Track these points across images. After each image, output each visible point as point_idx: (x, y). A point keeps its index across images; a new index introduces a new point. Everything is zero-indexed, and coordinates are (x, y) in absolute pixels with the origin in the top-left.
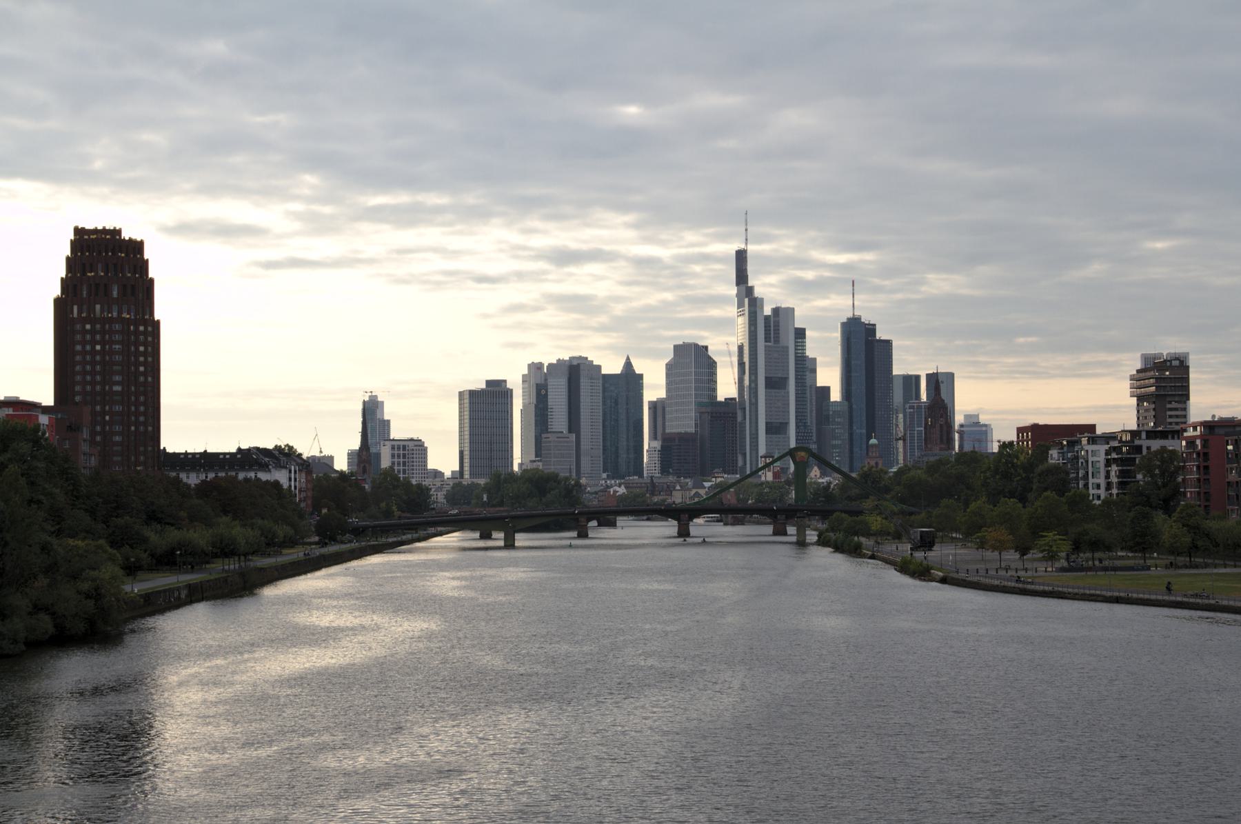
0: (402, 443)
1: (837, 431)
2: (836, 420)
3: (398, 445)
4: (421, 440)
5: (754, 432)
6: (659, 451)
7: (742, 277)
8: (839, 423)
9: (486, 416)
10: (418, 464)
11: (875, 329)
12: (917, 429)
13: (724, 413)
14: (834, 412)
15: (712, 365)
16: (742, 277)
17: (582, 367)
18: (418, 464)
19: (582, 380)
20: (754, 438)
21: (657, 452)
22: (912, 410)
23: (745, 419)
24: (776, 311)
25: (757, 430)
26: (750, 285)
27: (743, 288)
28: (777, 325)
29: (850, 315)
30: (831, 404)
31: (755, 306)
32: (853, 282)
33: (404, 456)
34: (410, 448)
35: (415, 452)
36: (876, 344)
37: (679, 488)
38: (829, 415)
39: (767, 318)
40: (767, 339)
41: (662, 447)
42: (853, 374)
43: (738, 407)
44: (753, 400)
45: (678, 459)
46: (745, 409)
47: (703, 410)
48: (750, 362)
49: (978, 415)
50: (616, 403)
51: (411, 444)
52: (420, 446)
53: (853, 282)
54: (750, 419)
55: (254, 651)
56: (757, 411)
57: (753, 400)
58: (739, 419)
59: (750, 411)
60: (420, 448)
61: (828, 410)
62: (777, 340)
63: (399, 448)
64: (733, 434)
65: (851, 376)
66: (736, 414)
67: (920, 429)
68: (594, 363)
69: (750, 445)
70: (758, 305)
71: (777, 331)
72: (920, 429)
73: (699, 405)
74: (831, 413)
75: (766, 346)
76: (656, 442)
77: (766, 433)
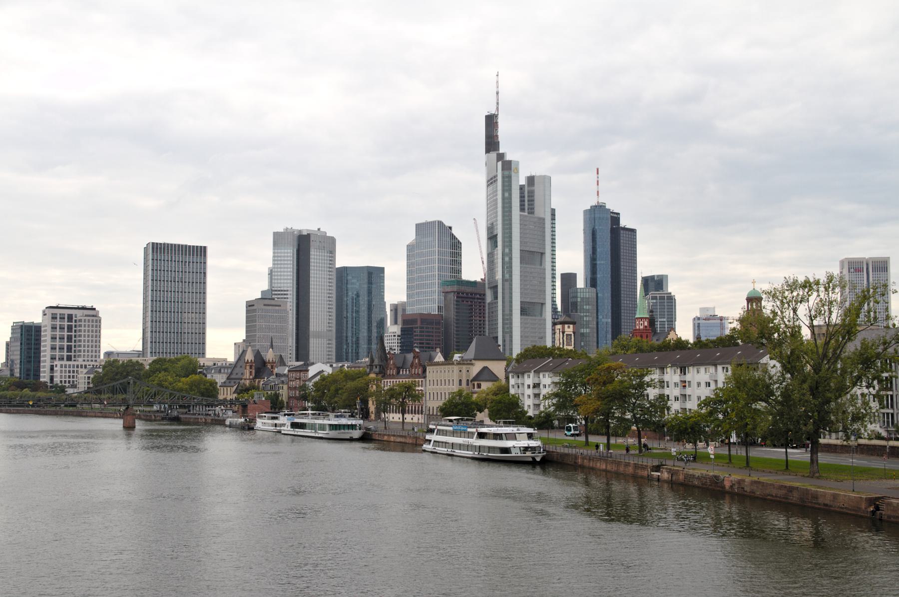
0: (67, 312)
1: (585, 319)
2: (585, 307)
3: (68, 315)
4: (95, 309)
5: (507, 312)
6: (398, 336)
7: (492, 143)
8: (588, 311)
9: (175, 277)
10: (87, 333)
11: (619, 218)
12: (665, 320)
13: (471, 294)
14: (582, 299)
15: (456, 245)
16: (492, 143)
17: (312, 238)
18: (87, 333)
19: (312, 252)
20: (507, 319)
21: (396, 337)
22: (655, 301)
23: (496, 298)
24: (531, 180)
25: (511, 311)
26: (501, 151)
27: (493, 155)
28: (531, 194)
29: (594, 203)
30: (579, 291)
31: (510, 169)
32: (598, 169)
33: (70, 328)
34: (78, 318)
35: (83, 323)
36: (622, 232)
37: (442, 359)
38: (577, 302)
39: (522, 188)
40: (522, 209)
41: (403, 330)
42: (598, 262)
43: (487, 286)
44: (507, 276)
45: (420, 343)
46: (496, 287)
47: (449, 289)
48: (504, 233)
49: (714, 308)
50: (358, 295)
51: (79, 313)
52: (93, 316)
53: (598, 169)
54: (503, 298)
55: (495, 394)
56: (511, 289)
57: (507, 276)
58: (489, 298)
59: (503, 289)
60: (94, 318)
61: (577, 297)
62: (531, 211)
63: (62, 318)
64: (480, 317)
65: (596, 264)
66: (484, 295)
67: (662, 320)
68: (328, 235)
69: (503, 328)
70: (513, 169)
71: (531, 201)
72: (662, 320)
73: (445, 284)
74: (579, 300)
75: (521, 215)
76: (396, 326)
77: (521, 314)
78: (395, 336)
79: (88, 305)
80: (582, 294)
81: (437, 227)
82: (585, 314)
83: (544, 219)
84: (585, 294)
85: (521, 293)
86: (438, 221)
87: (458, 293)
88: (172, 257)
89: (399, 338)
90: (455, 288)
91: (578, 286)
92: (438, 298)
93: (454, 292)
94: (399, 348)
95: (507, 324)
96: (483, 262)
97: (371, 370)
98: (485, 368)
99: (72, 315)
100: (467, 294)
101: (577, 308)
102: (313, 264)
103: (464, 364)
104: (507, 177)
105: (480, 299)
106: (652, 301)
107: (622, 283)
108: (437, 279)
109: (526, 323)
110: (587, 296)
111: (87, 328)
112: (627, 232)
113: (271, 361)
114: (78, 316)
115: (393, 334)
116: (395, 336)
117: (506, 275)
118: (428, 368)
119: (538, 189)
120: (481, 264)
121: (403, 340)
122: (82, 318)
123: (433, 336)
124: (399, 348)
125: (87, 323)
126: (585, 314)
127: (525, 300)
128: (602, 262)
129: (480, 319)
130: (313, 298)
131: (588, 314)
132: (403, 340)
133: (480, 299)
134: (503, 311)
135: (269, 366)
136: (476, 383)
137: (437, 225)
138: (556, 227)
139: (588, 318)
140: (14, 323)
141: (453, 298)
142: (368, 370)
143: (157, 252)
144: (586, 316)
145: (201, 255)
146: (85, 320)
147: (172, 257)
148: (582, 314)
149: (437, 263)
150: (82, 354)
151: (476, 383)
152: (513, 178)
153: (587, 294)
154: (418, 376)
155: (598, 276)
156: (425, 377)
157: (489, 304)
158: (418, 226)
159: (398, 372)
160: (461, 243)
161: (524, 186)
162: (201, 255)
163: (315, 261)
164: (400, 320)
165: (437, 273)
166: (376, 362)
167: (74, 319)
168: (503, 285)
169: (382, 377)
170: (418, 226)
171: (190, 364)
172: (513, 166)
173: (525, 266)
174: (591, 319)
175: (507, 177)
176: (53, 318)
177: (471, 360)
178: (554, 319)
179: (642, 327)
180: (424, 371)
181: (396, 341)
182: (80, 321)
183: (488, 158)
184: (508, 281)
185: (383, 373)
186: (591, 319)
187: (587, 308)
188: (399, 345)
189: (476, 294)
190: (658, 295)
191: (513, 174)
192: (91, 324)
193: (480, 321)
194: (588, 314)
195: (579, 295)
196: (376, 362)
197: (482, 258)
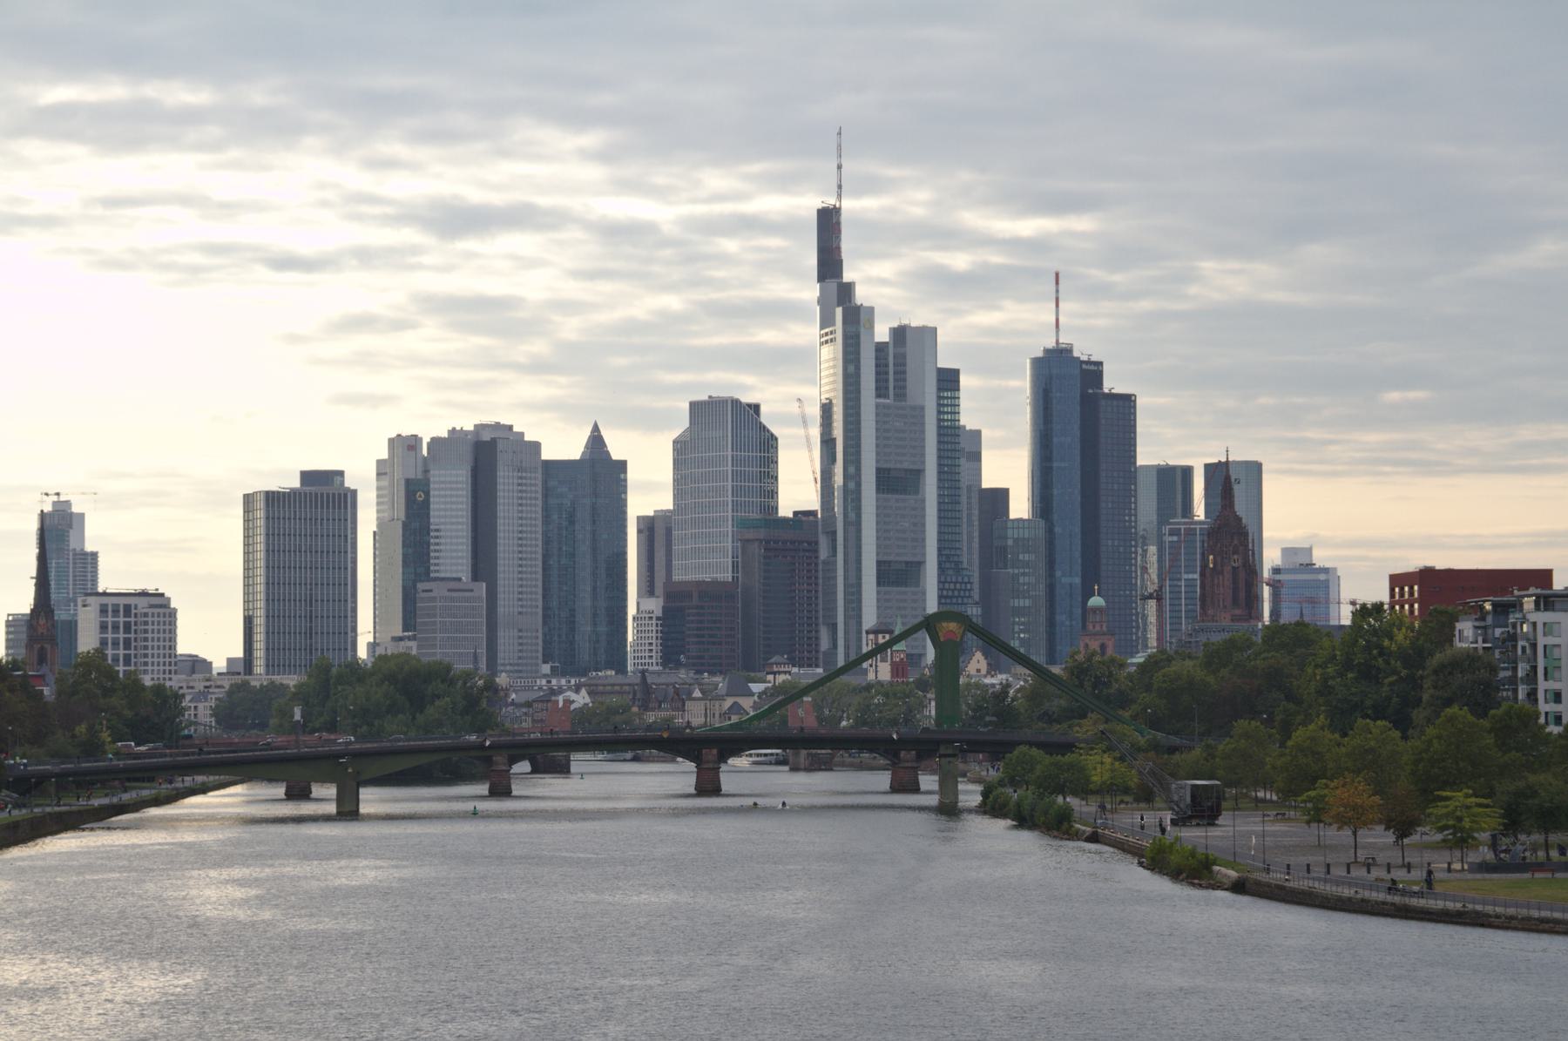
0: (122, 601)
1: (1021, 580)
2: (1021, 557)
4: (162, 595)
6: (658, 619)
7: (829, 264)
8: (1027, 564)
11: (1102, 371)
12: (1185, 576)
13: (793, 542)
14: (1016, 540)
15: (767, 444)
17: (500, 446)
19: (500, 473)
21: (654, 622)
22: (1175, 538)
24: (900, 333)
25: (859, 578)
27: (832, 285)
28: (901, 362)
29: (1051, 344)
30: (1010, 525)
31: (857, 322)
32: (1057, 275)
34: (141, 610)
36: (1103, 402)
37: (700, 695)
39: (881, 348)
40: (881, 391)
42: (1055, 465)
44: (852, 516)
46: (834, 533)
47: (750, 535)
53: (1057, 275)
54: (846, 554)
58: (823, 554)
59: (845, 539)
61: (1006, 538)
62: (901, 394)
63: (116, 612)
66: (817, 543)
67: (1191, 576)
71: (901, 374)
72: (1191, 576)
73: (742, 524)
74: (1010, 542)
77: (879, 584)
78: (651, 618)
79: (151, 588)
80: (1016, 531)
81: (730, 435)
82: (1021, 570)
83: (922, 408)
84: (1021, 531)
85: (878, 546)
86: (732, 401)
87: (768, 542)
88: (295, 512)
89: (659, 622)
90: (762, 534)
91: (1013, 515)
92: (733, 547)
93: (761, 541)
94: (659, 641)
95: (853, 609)
96: (816, 479)
97: (634, 703)
98: (735, 703)
99: (130, 606)
100: (784, 542)
101: (1006, 557)
102: (502, 494)
103: (717, 700)
104: (852, 337)
105: (809, 551)
106: (1170, 539)
107: (1103, 505)
108: (730, 511)
109: (887, 600)
110: (1026, 536)
111: (156, 627)
112: (1115, 403)
113: (504, 687)
114: (139, 607)
115: (647, 616)
116: (651, 618)
117: (850, 515)
118: (687, 702)
119: (910, 348)
120: (813, 482)
121: (666, 629)
122: (145, 610)
123: (720, 621)
124: (659, 641)
125: (156, 619)
126: (1021, 570)
127: (886, 558)
128: (1063, 465)
129: (810, 588)
130: (502, 548)
131: (1027, 570)
132: (666, 629)
133: (809, 551)
134: (846, 578)
135: (502, 694)
136: (727, 716)
137: (730, 408)
138: (961, 396)
139: (1027, 578)
140: (9, 615)
141: (757, 550)
142: (631, 703)
143: (273, 506)
144: (1024, 574)
145: (340, 508)
146: (153, 614)
147: (295, 512)
148: (1016, 571)
149: (730, 450)
150: (150, 668)
151: (727, 716)
152: (863, 338)
153: (1026, 531)
154: (677, 709)
155: (1055, 492)
156: (684, 711)
157: (824, 562)
158: (695, 407)
159: (660, 706)
160: (776, 439)
161: (886, 344)
162: (340, 508)
163: (506, 488)
164: (659, 588)
165: (730, 499)
166: (639, 696)
167: (133, 611)
168: (845, 531)
169: (644, 710)
170: (695, 407)
171: (686, 728)
172: (863, 317)
173: (885, 496)
174: (1033, 580)
175: (852, 337)
176: (102, 611)
177: (723, 696)
178: (944, 583)
179: (898, 660)
180: (684, 705)
181: (654, 628)
182: (146, 615)
183: (822, 290)
184: (854, 525)
185: (645, 707)
186: (1033, 580)
187: (1027, 558)
188: (659, 635)
189: (801, 542)
190: (1182, 527)
191: (862, 330)
192: (162, 619)
193: (809, 591)
194: (1027, 570)
195: (1010, 532)
196: (639, 696)
197: (814, 472)
